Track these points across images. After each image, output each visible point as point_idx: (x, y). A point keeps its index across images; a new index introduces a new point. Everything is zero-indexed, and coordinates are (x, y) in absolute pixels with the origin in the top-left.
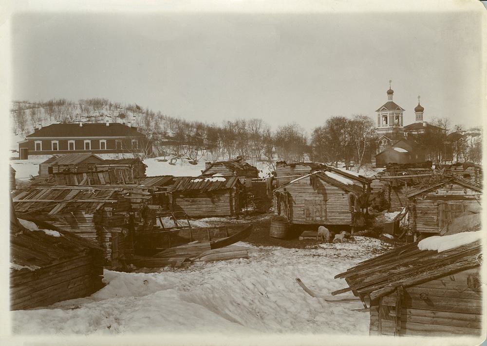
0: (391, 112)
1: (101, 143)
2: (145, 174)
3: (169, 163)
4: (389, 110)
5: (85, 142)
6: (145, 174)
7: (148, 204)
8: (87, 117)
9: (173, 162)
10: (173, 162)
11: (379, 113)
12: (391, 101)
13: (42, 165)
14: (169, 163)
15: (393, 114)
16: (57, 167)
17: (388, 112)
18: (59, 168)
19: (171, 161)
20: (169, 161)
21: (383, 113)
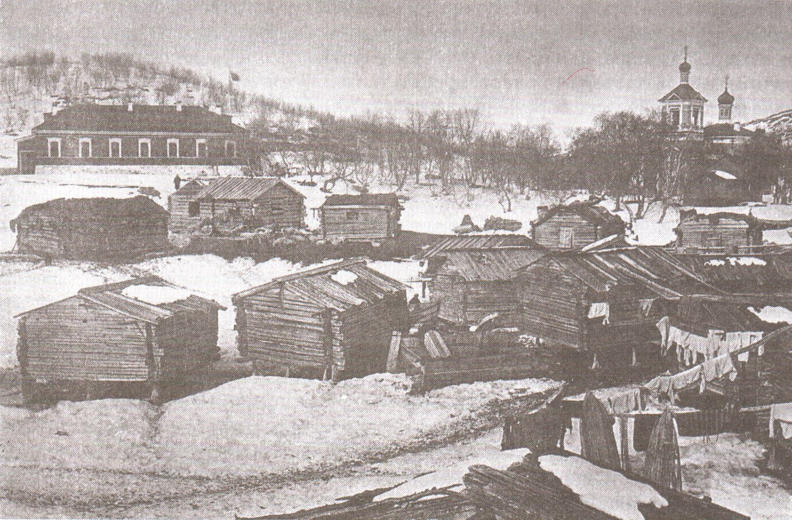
0: (687, 103)
1: (170, 144)
2: (399, 222)
3: (321, 189)
4: (684, 99)
5: (141, 141)
6: (399, 222)
7: (662, 307)
8: (109, 90)
9: (328, 188)
10: (328, 188)
11: (664, 104)
12: (686, 83)
13: (173, 197)
14: (321, 189)
15: (689, 107)
16: (211, 204)
17: (681, 104)
18: (213, 206)
19: (325, 187)
20: (321, 185)
21: (674, 104)
